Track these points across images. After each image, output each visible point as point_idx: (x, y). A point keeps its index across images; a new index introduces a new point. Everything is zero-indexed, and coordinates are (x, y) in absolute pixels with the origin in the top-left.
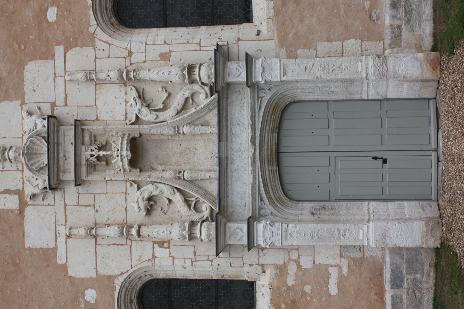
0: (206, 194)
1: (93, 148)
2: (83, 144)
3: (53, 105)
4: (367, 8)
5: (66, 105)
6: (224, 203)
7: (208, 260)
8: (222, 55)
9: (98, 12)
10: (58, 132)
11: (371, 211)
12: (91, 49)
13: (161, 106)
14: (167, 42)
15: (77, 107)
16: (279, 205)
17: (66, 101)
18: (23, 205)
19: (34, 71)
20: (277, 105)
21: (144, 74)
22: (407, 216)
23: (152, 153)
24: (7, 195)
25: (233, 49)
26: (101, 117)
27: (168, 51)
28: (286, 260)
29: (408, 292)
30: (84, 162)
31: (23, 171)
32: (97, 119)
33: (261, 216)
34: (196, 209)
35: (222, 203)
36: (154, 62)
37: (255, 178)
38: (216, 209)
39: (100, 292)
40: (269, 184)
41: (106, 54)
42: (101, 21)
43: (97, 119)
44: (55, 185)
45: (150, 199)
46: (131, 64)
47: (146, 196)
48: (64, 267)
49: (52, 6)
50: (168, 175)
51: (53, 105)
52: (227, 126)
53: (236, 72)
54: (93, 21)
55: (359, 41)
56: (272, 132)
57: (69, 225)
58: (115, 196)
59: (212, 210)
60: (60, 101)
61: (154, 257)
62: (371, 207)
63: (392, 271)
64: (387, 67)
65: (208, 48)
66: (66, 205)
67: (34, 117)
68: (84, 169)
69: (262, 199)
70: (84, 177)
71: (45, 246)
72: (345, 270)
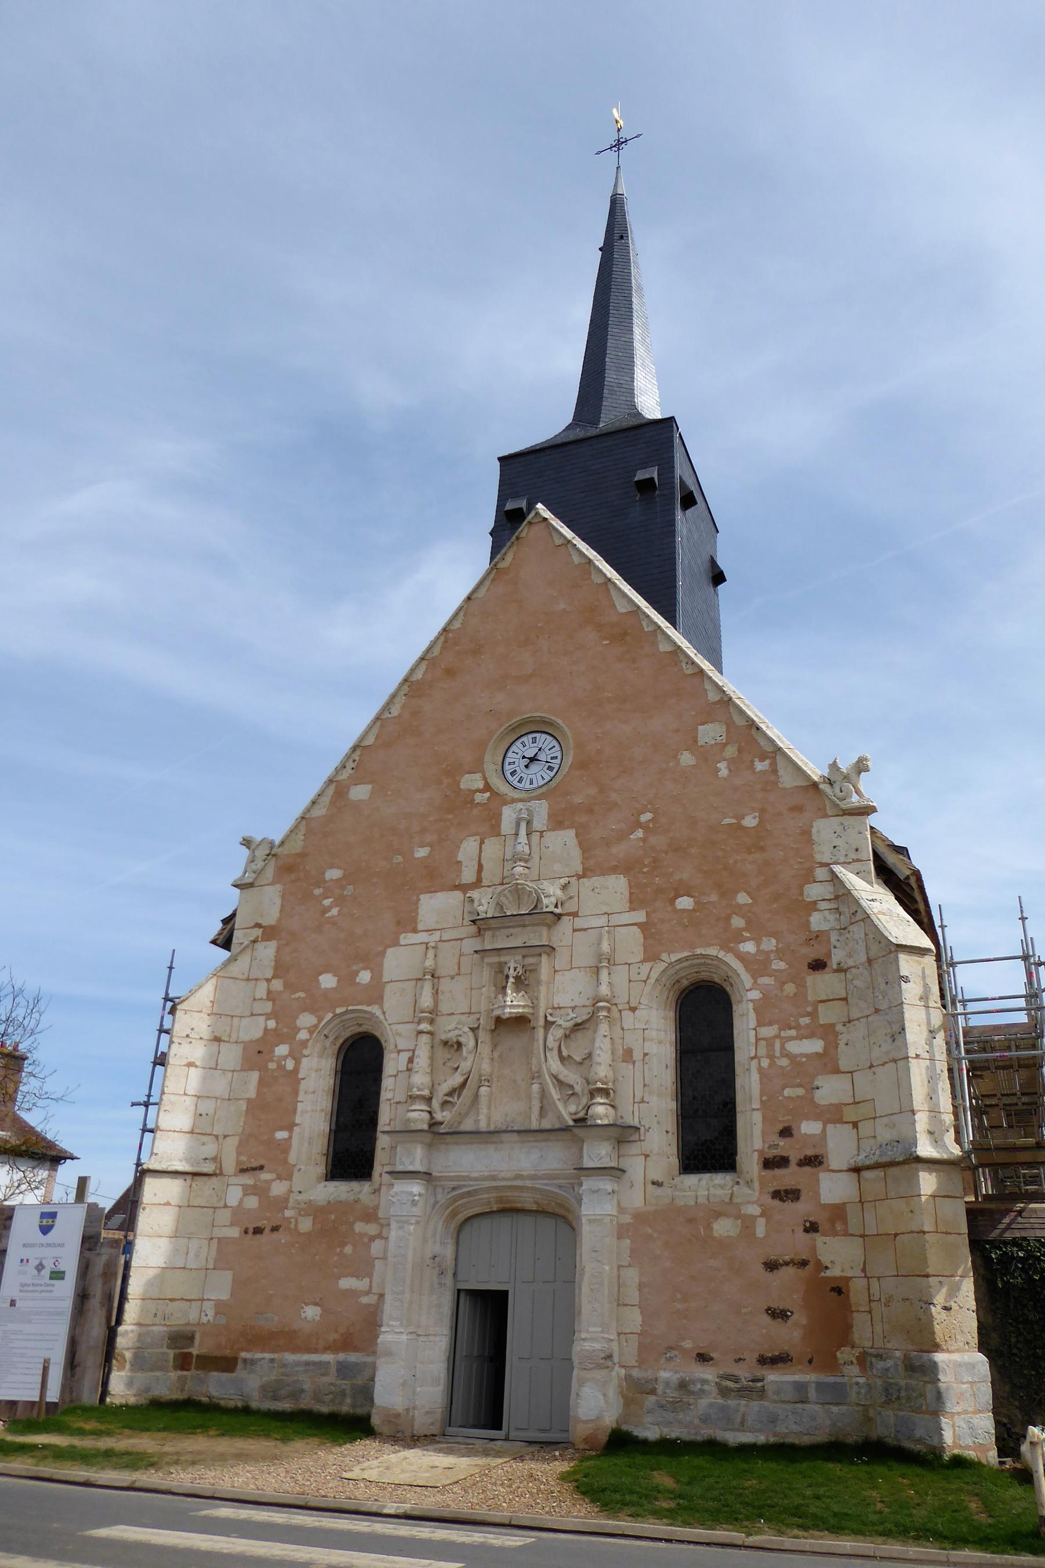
0: (462, 1116)
1: (519, 969)
2: (524, 957)
3: (575, 915)
4: (683, 1344)
5: (575, 930)
6: (449, 1139)
7: (142, 1174)
8: (623, 1134)
9: (689, 962)
10: (538, 925)
11: (432, 1338)
12: (640, 957)
13: (565, 1053)
14: (647, 1057)
15: (143, 1108)
16: (448, 1211)
17: (579, 930)
18: (464, 888)
19: (618, 885)
20: (568, 1210)
21: (603, 1028)
22: (419, 1389)
23: (512, 1042)
24: (476, 867)
25: (634, 1149)
26: (558, 977)
27: (635, 1058)
28: (382, 1221)
29: (332, 1384)
30: (503, 959)
31: (502, 884)
32: (555, 971)
33: (435, 1187)
34: (445, 1104)
35: (448, 1136)
36: (621, 1041)
37: (476, 1179)
38: (442, 1129)
39: (368, 986)
40: (472, 1199)
41: (634, 977)
42: (677, 967)
43: (555, 971)
44: (480, 925)
45: (459, 1045)
46: (620, 1011)
47: (462, 1040)
48: (396, 943)
49: (695, 903)
50: (486, 1067)
51: (575, 915)
52: (539, 1141)
53: (598, 1153)
54: (674, 957)
55: (638, 1330)
56: (536, 1203)
57: (440, 945)
58: (464, 1000)
59: (442, 1123)
60: (579, 923)
61: (399, 1052)
62: (437, 1339)
63: (357, 1364)
64: (591, 1369)
65: (636, 1114)
66: (462, 939)
67: (559, 893)
68: (495, 959)
69: (454, 1189)
70: (487, 960)
71: (420, 918)
72: (364, 1300)
